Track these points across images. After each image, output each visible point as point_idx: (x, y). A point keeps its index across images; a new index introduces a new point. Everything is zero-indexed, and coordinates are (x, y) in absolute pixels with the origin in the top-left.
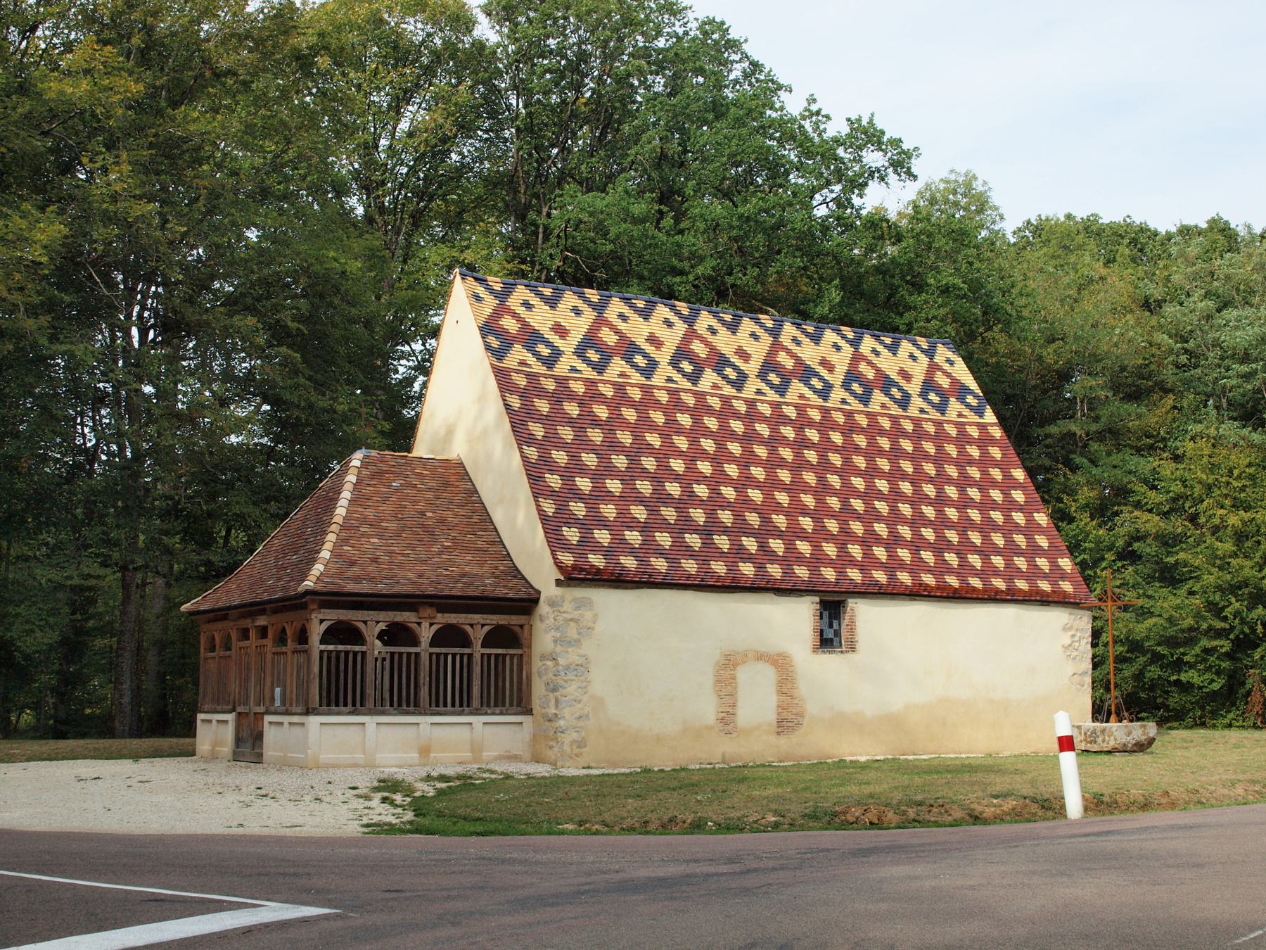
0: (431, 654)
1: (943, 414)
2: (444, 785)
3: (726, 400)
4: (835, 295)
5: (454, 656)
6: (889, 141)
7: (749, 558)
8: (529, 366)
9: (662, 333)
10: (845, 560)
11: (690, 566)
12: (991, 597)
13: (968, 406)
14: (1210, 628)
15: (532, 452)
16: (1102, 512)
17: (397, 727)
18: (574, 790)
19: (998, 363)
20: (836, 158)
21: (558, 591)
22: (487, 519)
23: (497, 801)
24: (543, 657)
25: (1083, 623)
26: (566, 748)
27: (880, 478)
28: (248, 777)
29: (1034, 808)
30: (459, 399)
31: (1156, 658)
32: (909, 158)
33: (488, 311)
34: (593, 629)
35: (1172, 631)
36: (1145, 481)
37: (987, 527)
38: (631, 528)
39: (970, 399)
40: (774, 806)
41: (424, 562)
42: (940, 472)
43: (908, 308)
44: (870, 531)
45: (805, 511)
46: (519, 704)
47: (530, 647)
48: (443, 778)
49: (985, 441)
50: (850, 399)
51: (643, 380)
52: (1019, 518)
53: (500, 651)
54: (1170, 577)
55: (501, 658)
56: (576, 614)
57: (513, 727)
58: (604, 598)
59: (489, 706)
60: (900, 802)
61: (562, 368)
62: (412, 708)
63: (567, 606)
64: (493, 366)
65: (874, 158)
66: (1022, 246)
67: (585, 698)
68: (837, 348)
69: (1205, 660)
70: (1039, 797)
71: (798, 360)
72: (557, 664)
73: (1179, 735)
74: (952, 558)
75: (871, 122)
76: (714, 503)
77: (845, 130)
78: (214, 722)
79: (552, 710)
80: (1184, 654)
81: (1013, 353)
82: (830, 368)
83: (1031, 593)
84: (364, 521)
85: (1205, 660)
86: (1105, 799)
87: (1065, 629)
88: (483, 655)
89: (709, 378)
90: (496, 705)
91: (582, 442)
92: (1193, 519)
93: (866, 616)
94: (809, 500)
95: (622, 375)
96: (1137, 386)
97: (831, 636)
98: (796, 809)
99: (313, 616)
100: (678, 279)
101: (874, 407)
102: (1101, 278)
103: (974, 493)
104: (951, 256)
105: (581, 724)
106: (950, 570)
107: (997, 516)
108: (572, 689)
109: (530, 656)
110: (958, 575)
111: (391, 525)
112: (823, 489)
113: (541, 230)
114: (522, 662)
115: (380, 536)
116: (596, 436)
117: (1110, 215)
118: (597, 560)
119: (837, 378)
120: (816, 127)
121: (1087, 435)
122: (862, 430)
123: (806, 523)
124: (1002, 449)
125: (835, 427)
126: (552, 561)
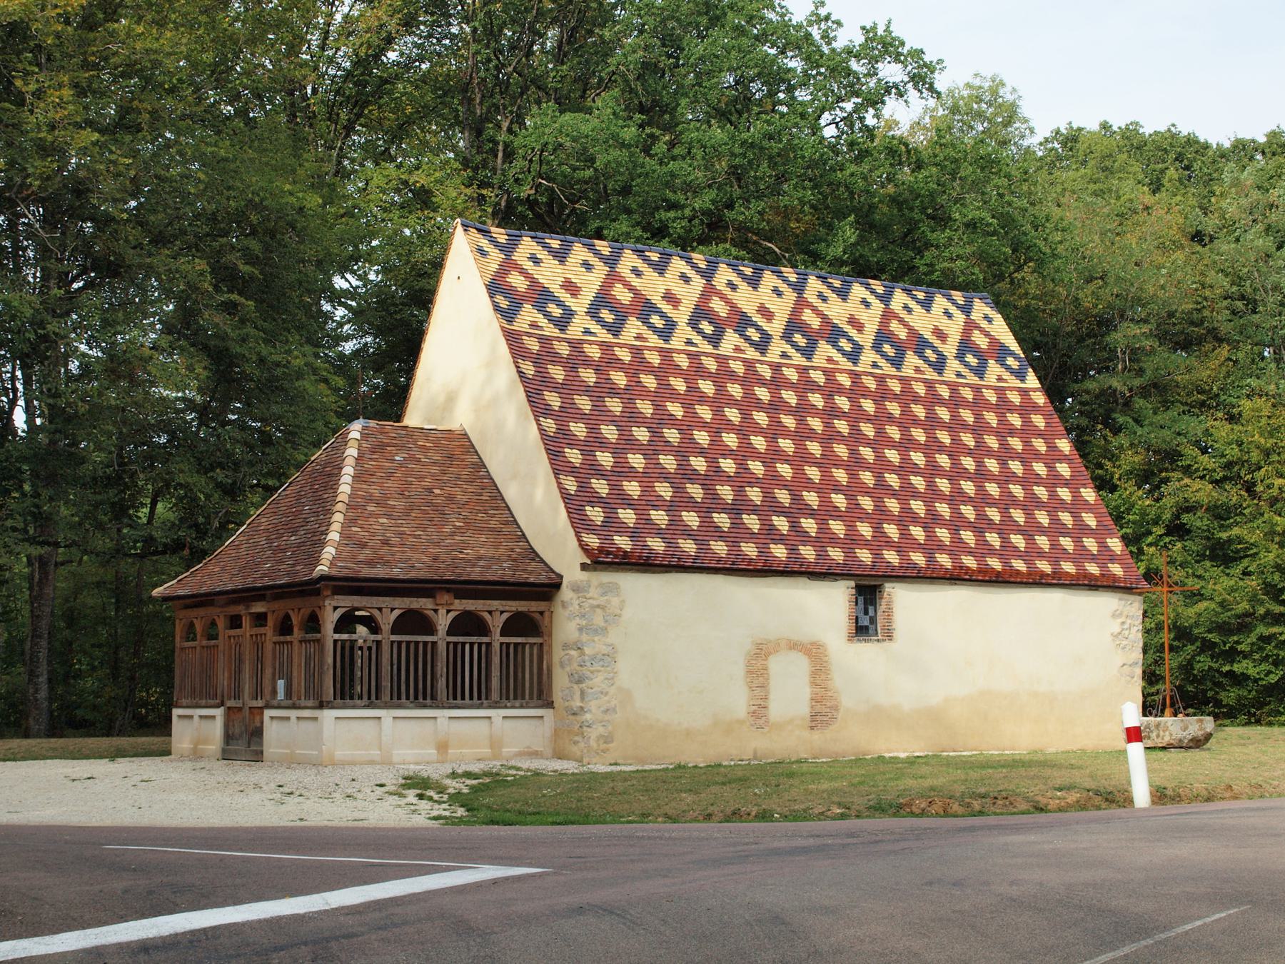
0: (448, 643)
1: (981, 378)
2: (474, 782)
3: (750, 364)
4: (848, 232)
5: (472, 645)
6: (909, 53)
7: (781, 539)
8: (540, 328)
9: (679, 289)
10: (880, 542)
11: (720, 548)
12: (1035, 581)
13: (1008, 368)
14: (1268, 613)
15: (550, 425)
16: (1148, 477)
17: (413, 722)
18: (620, 786)
19: (1028, 306)
20: (849, 72)
21: (584, 576)
22: (498, 496)
23: (544, 796)
24: (566, 646)
25: (1133, 607)
26: (593, 743)
27: (916, 450)
28: (244, 773)
29: (1098, 800)
30: (464, 367)
31: (1207, 646)
32: (932, 73)
33: (494, 267)
34: (620, 616)
35: (1224, 617)
36: (1197, 443)
37: (1031, 504)
38: (656, 507)
39: (1010, 361)
40: (835, 799)
41: (437, 544)
42: (980, 444)
43: (928, 245)
44: (906, 509)
45: (837, 488)
46: (539, 697)
47: (550, 635)
48: (468, 775)
49: (1027, 408)
50: (882, 363)
51: (661, 343)
52: (1064, 494)
53: (519, 640)
54: (1223, 554)
55: (520, 648)
56: (602, 600)
57: (529, 721)
58: (633, 584)
59: (508, 698)
60: (963, 794)
61: (575, 331)
62: (428, 701)
63: (593, 592)
64: (502, 328)
65: (891, 71)
66: (1052, 162)
67: (612, 690)
68: (867, 304)
69: (1261, 649)
70: (1102, 790)
71: (824, 318)
72: (583, 654)
73: (1234, 732)
74: (993, 539)
75: (887, 30)
76: (742, 479)
77: (859, 39)
78: (196, 718)
79: (577, 703)
80: (1238, 643)
81: (1045, 294)
82: (859, 327)
83: (1078, 576)
84: (370, 499)
85: (1261, 649)
86: (1169, 793)
87: (1114, 616)
88: (502, 644)
89: (731, 340)
90: (515, 698)
91: (601, 413)
92: (1250, 488)
93: (904, 601)
94: (841, 475)
95: (639, 337)
96: (1187, 335)
97: (866, 623)
98: (859, 802)
99: (327, 602)
100: (672, 214)
101: (908, 371)
102: (1147, 208)
103: (1016, 466)
104: (977, 186)
105: (607, 717)
106: (991, 551)
107: (1041, 492)
108: (598, 681)
109: (550, 646)
110: (1001, 557)
111: (400, 504)
112: (855, 464)
113: (501, 148)
114: (542, 651)
115: (389, 516)
116: (615, 405)
117: (1151, 125)
118: (623, 542)
119: (866, 339)
120: (825, 36)
121: (1131, 390)
122: (895, 397)
123: (839, 500)
124: (1047, 417)
125: (866, 394)
126: (576, 543)
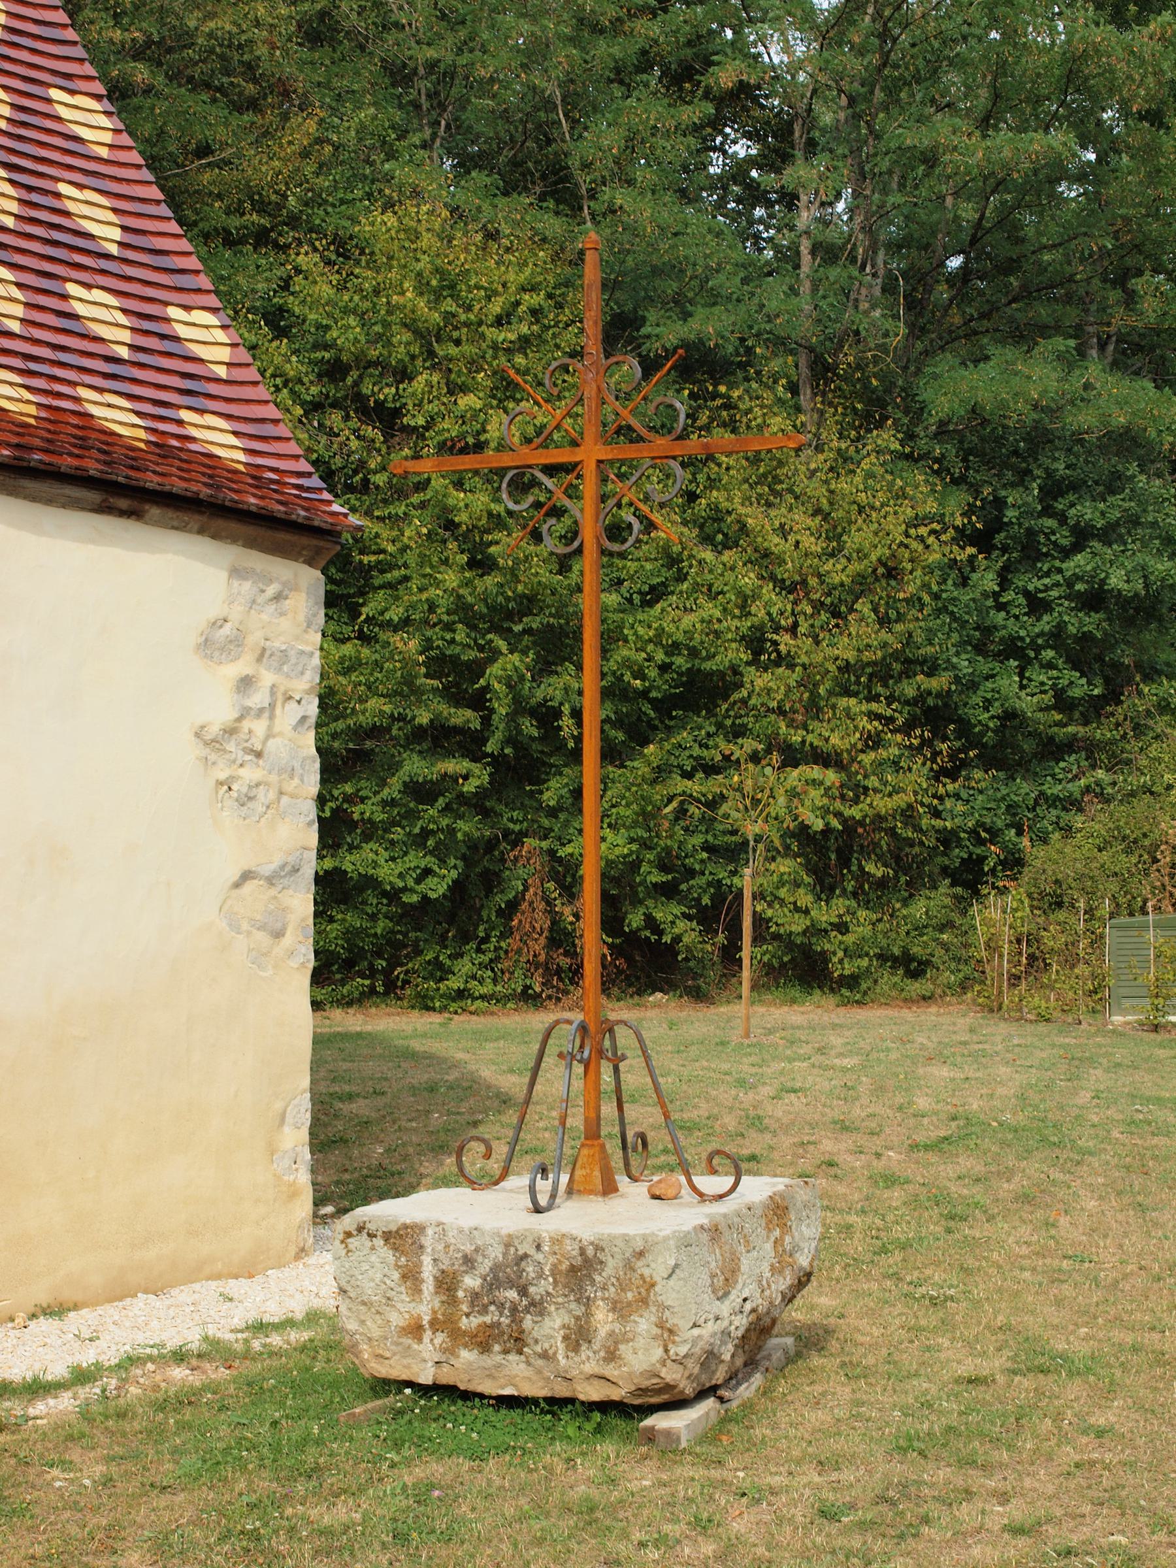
87: (214, 644)
